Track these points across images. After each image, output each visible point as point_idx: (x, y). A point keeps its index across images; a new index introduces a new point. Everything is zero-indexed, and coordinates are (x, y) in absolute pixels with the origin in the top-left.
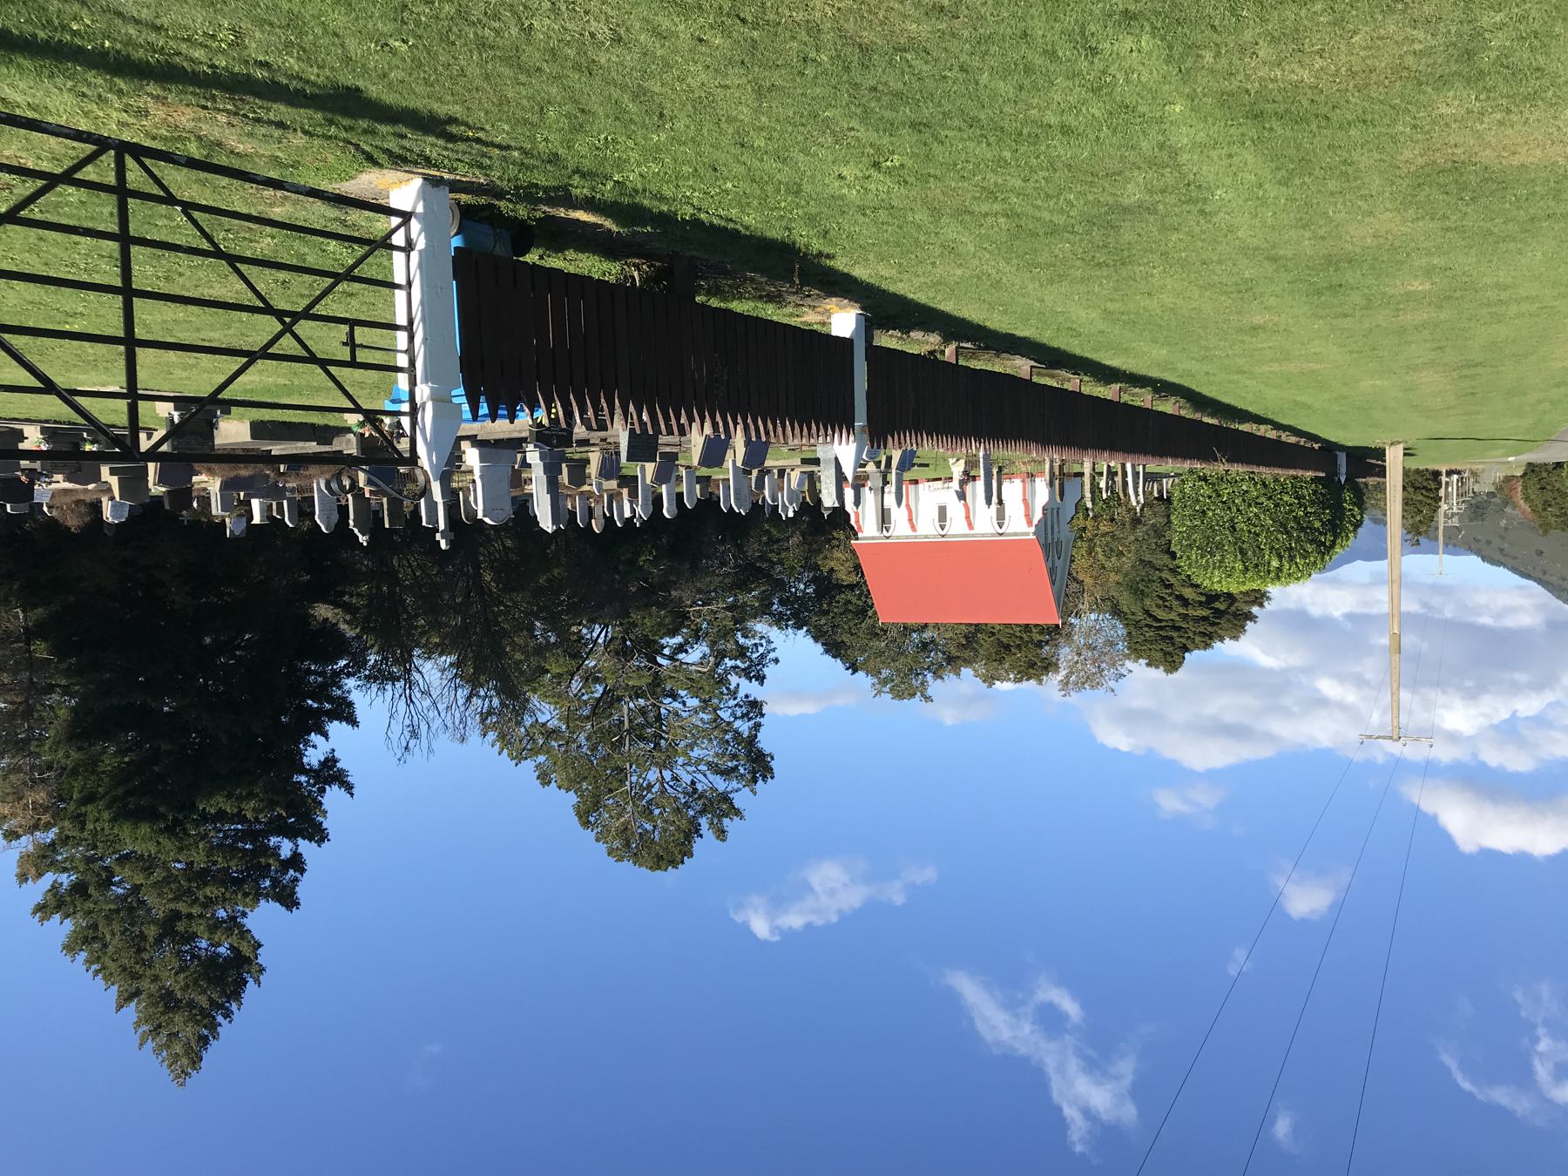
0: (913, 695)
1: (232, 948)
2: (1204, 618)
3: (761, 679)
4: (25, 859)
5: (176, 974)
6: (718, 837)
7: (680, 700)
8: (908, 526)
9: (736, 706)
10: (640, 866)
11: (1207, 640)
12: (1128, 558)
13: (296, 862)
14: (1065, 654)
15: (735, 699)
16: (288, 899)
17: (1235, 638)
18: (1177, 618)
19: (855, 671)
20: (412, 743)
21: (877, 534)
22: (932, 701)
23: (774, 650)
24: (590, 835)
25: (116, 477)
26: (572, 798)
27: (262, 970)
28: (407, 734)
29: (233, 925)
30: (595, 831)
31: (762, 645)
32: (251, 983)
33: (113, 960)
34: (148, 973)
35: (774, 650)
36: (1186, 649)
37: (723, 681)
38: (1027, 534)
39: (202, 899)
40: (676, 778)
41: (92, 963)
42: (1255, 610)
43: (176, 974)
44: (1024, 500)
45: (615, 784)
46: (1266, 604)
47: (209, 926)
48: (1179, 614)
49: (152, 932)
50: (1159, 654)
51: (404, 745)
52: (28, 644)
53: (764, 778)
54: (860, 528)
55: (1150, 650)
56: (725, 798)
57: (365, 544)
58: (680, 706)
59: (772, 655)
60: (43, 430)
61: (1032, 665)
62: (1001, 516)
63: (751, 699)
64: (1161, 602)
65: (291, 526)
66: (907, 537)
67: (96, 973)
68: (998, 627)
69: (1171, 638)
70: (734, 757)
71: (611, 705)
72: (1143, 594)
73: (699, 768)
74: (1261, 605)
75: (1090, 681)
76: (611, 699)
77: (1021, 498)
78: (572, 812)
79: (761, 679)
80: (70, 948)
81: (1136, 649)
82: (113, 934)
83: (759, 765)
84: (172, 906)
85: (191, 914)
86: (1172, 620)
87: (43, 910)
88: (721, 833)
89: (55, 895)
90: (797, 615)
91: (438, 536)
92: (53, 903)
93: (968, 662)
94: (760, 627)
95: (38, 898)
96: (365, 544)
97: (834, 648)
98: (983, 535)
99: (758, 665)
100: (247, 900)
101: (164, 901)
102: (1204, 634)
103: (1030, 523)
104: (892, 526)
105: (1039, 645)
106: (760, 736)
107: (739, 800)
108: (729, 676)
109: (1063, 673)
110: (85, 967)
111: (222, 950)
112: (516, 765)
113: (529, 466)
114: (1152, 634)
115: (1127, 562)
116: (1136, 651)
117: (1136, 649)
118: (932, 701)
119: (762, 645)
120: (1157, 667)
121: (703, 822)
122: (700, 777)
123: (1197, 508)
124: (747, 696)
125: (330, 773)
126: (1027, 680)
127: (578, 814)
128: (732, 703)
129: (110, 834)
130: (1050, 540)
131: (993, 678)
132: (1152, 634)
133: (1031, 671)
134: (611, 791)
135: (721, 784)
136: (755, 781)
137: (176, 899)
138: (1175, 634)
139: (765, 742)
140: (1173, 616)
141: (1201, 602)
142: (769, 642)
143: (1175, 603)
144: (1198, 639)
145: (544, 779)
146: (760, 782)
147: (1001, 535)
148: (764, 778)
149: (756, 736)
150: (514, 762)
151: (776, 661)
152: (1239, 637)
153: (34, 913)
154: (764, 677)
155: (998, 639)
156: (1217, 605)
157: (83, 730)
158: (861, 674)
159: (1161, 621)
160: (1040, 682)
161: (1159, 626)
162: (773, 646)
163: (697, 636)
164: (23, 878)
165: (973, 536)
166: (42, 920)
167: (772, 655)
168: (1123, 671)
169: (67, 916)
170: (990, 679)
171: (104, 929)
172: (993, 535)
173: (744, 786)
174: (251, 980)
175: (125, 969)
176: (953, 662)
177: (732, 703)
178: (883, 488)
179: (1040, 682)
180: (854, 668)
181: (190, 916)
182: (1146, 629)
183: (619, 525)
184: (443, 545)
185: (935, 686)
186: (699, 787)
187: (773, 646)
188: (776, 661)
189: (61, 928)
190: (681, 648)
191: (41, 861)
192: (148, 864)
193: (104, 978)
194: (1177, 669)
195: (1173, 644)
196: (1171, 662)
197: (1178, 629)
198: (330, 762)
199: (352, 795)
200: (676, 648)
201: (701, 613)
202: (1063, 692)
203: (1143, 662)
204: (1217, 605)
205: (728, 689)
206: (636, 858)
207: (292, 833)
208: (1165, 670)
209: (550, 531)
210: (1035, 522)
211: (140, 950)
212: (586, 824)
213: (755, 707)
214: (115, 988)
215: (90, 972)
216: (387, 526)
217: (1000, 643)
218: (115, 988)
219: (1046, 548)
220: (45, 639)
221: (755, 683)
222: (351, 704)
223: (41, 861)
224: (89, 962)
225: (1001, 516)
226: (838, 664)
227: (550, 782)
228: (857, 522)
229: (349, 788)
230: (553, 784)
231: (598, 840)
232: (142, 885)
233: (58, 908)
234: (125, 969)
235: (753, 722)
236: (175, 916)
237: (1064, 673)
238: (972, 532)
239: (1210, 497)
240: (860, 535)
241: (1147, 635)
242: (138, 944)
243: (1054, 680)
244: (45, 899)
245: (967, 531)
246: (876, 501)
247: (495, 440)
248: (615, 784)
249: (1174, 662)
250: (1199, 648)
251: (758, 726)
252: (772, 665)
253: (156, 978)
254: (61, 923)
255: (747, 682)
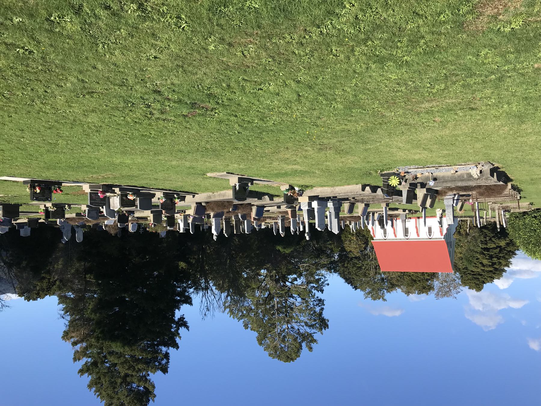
0: (379, 299)
1: (145, 387)
2: (491, 271)
3: (322, 291)
4: (77, 352)
5: (126, 397)
6: (309, 350)
7: (295, 298)
8: (416, 234)
9: (314, 301)
10: (281, 360)
11: (492, 279)
12: (465, 248)
13: (167, 356)
14: (436, 283)
15: (314, 298)
16: (165, 370)
17: (499, 278)
18: (481, 271)
19: (356, 289)
20: (207, 312)
21: (404, 238)
22: (386, 301)
23: (327, 280)
24: (262, 348)
25: (152, 214)
26: (256, 334)
27: (155, 396)
28: (205, 310)
29: (144, 379)
30: (264, 347)
31: (322, 279)
32: (151, 401)
33: (105, 392)
34: (116, 396)
35: (327, 280)
36: (484, 283)
37: (310, 292)
38: (442, 239)
39: (137, 369)
40: (292, 328)
41: (97, 392)
42: (506, 268)
43: (126, 397)
44: (416, 227)
45: (272, 329)
46: (510, 266)
47: (138, 379)
48: (481, 270)
49: (119, 381)
50: (474, 284)
51: (204, 313)
52: (85, 275)
53: (325, 328)
54: (374, 236)
55: (470, 283)
56: (310, 335)
57: (215, 240)
58: (295, 300)
59: (326, 282)
60: (164, 193)
61: (424, 288)
62: (385, 233)
63: (319, 298)
64: (475, 265)
65: (192, 233)
66: (393, 239)
67: (98, 396)
68: (412, 274)
69: (478, 278)
70: (315, 320)
71: (270, 300)
72: (471, 262)
73: (301, 324)
74: (509, 267)
75: (447, 294)
76: (271, 297)
77: (415, 226)
78: (256, 339)
79: (322, 291)
80: (90, 386)
81: (465, 282)
82: (106, 382)
83: (323, 324)
84: (126, 372)
85: (132, 375)
86: (478, 272)
87: (82, 372)
88: (311, 349)
89: (87, 366)
90: (332, 267)
91: (306, 235)
92: (85, 369)
93: (399, 286)
94: (323, 272)
95: (80, 367)
96: (215, 240)
97: (349, 280)
98: (423, 239)
99: (321, 286)
100: (152, 370)
101: (124, 370)
102: (491, 277)
103: (442, 234)
104: (409, 234)
105: (427, 280)
106: (324, 312)
107: (315, 337)
108: (312, 290)
109: (436, 291)
110: (94, 393)
111: (141, 388)
112: (238, 321)
113: (302, 210)
114: (471, 277)
115: (464, 250)
116: (464, 283)
117: (465, 282)
118: (386, 301)
119: (322, 279)
120: (473, 289)
121: (304, 344)
122: (301, 327)
123: (532, 228)
124: (317, 297)
125: (182, 322)
126: (422, 293)
127: (258, 340)
128: (313, 300)
129: (108, 344)
130: (448, 241)
131: (409, 292)
132: (471, 277)
133: (424, 290)
134: (270, 332)
135: (308, 330)
136: (321, 329)
137: (129, 369)
138: (480, 277)
139: (325, 315)
140: (479, 270)
141: (489, 265)
142: (325, 277)
143: (480, 265)
144: (489, 279)
145: (246, 326)
146: (323, 330)
147: (430, 239)
148: (325, 328)
149: (322, 313)
150: (238, 320)
151: (328, 284)
152: (500, 278)
153: (79, 373)
154: (323, 290)
155: (411, 278)
156: (495, 266)
157: (101, 305)
158: (359, 290)
159: (474, 272)
160: (427, 294)
161: (473, 274)
162: (326, 279)
163: (300, 275)
164: (75, 359)
165: (419, 239)
166: (81, 375)
167: (326, 282)
168: (459, 290)
169: (90, 374)
170: (408, 293)
171: (103, 380)
172: (427, 239)
173: (318, 331)
174: (151, 400)
175: (108, 395)
176: (392, 286)
177: (313, 300)
178: (405, 220)
179: (427, 294)
180: (356, 288)
181: (132, 376)
182: (469, 275)
183: (292, 234)
184: (307, 238)
185: (387, 296)
186: (301, 331)
187: (326, 279)
188: (328, 284)
189: (87, 378)
190: (295, 279)
191: (83, 353)
192: (120, 355)
193: (101, 398)
194: (481, 290)
195: (479, 281)
196: (479, 288)
197: (481, 275)
198: (182, 319)
199: (188, 330)
200: (293, 279)
201: (302, 267)
202: (437, 298)
203: (467, 287)
204: (495, 266)
205: (312, 295)
206: (279, 357)
207: (167, 345)
208: (476, 291)
209: (336, 233)
210: (444, 234)
211: (114, 388)
212: (261, 344)
213: (321, 302)
214: (105, 401)
215: (96, 395)
216: (235, 233)
217: (412, 279)
218: (105, 401)
219: (447, 243)
220: (91, 273)
221: (320, 292)
222: (191, 298)
223: (83, 353)
224: (96, 391)
225: (385, 233)
226: (349, 287)
227: (248, 328)
228: (373, 233)
229: (187, 328)
230: (249, 329)
231: (265, 350)
232: (117, 363)
233: (87, 371)
234: (108, 395)
235: (320, 307)
236: (127, 375)
237: (437, 291)
238: (419, 238)
239: (537, 224)
240: (374, 238)
241: (469, 277)
242: (113, 384)
243: (432, 294)
244: (82, 368)
245: (417, 237)
246: (403, 225)
247: (327, 197)
248: (272, 329)
249: (480, 287)
250: (489, 282)
251: (322, 309)
252: (326, 286)
253: (119, 399)
254: (88, 377)
255: (317, 292)
